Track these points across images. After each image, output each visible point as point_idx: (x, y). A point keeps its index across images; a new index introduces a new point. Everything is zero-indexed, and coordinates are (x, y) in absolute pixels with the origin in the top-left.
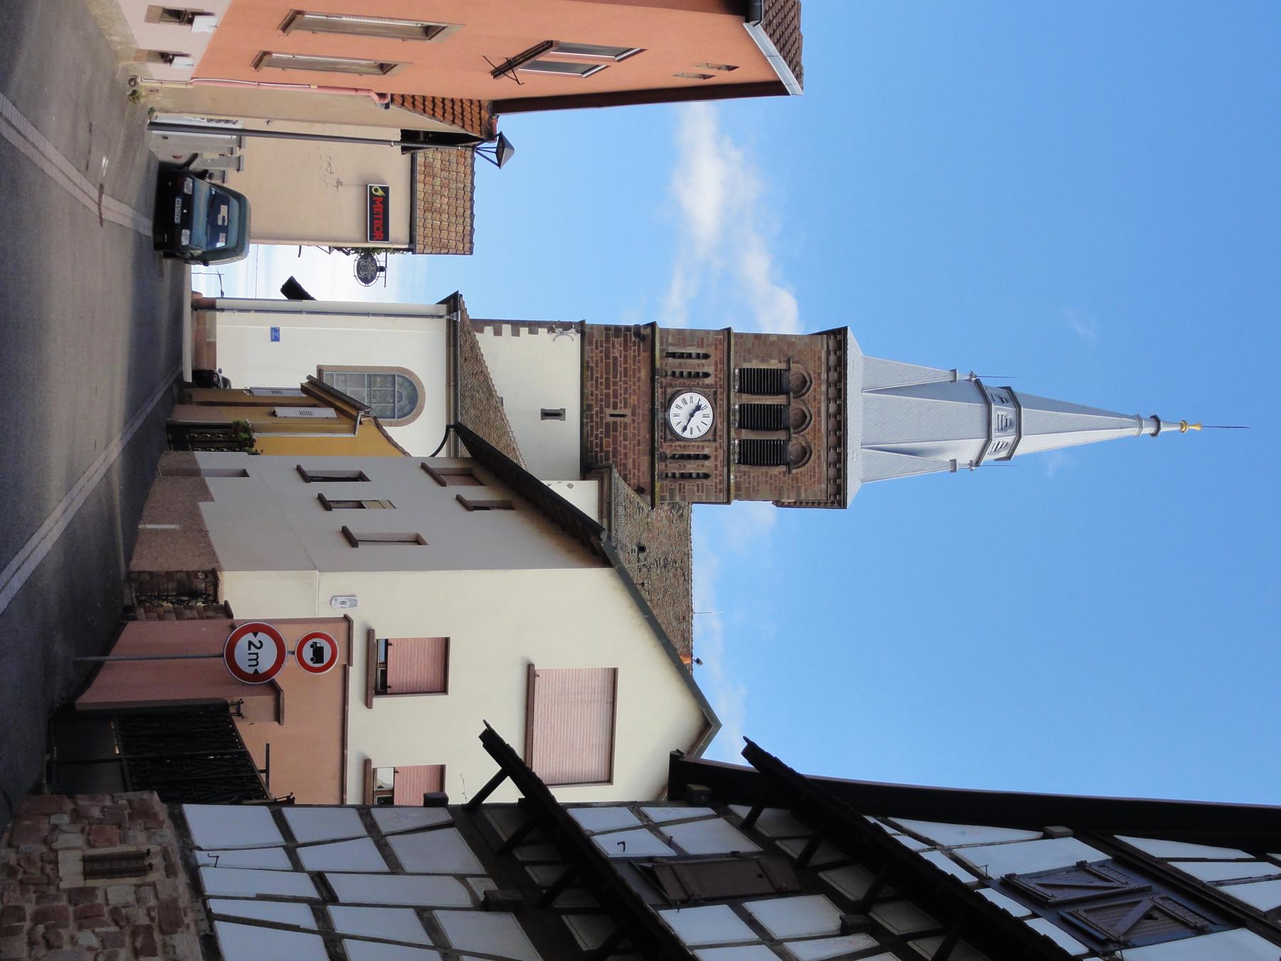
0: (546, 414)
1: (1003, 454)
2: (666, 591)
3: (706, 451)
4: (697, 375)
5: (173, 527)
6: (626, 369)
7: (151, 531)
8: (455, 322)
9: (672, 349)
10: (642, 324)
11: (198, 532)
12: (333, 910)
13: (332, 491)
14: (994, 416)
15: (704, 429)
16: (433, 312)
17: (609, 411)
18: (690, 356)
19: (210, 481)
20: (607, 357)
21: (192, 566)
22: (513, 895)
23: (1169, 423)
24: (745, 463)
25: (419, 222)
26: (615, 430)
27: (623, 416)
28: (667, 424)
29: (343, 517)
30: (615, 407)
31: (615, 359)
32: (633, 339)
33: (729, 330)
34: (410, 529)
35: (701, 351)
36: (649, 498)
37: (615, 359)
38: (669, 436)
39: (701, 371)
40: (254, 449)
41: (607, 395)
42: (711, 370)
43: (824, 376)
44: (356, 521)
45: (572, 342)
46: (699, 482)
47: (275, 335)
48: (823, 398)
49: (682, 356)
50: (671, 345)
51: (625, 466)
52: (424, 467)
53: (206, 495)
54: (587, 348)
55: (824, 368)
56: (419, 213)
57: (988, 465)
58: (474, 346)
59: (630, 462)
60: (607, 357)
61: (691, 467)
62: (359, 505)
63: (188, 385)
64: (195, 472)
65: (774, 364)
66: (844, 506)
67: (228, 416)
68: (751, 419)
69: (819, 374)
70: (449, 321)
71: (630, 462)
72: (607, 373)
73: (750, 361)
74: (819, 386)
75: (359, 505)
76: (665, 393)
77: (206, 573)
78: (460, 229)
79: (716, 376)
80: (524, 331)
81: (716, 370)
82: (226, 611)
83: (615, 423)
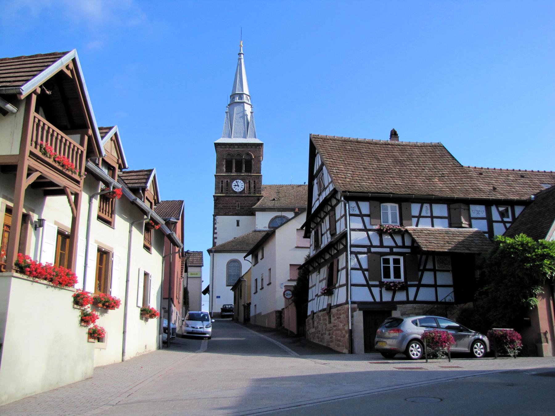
0: (238, 225)
1: (249, 97)
2: (285, 192)
3: (248, 181)
4: (227, 184)
5: (267, 320)
6: (226, 204)
7: (268, 324)
8: (215, 251)
9: (220, 191)
10: (213, 199)
11: (268, 315)
12: (319, 295)
13: (259, 287)
14: (238, 101)
15: (242, 182)
16: (212, 256)
17: (237, 208)
18: (222, 186)
19: (257, 313)
20: (223, 209)
21: (275, 316)
22: (318, 269)
23: (240, 51)
24: (251, 171)
25: (196, 265)
26: (242, 206)
27: (238, 204)
28: (241, 192)
29: (265, 285)
30: (236, 206)
31: (223, 206)
32: (218, 201)
33: (215, 175)
34: (268, 272)
35: (221, 183)
36: (260, 197)
37: (223, 206)
38: (244, 192)
39: (226, 183)
40: (41, 174)
41: (233, 208)
42: (226, 180)
43: (227, 149)
44: (266, 282)
45: (219, 218)
46: (256, 183)
47: (218, 297)
48: (233, 149)
49: (222, 188)
50: (219, 191)
51: (251, 204)
52: (254, 266)
53: (260, 314)
54: (220, 214)
55: (225, 149)
56: (194, 265)
57: (251, 102)
58: (221, 246)
59: (251, 202)
60: (223, 209)
61: (252, 186)
62: (262, 280)
63: (233, 319)
64: (255, 316)
65: (224, 163)
66: (263, 143)
67: (242, 308)
68: (239, 170)
69: (227, 150)
70: (214, 253)
71: (251, 202)
72: (227, 208)
73: (223, 170)
74: (230, 150)
75: (262, 280)
76: (232, 193)
77: (276, 313)
78: (197, 255)
79: (228, 179)
80: (216, 231)
81: (226, 179)
82: (283, 309)
83: (240, 206)
